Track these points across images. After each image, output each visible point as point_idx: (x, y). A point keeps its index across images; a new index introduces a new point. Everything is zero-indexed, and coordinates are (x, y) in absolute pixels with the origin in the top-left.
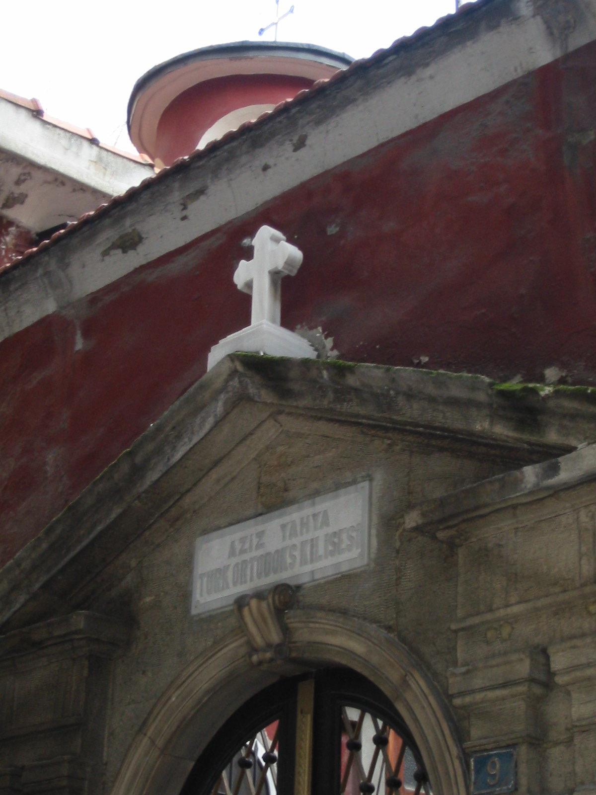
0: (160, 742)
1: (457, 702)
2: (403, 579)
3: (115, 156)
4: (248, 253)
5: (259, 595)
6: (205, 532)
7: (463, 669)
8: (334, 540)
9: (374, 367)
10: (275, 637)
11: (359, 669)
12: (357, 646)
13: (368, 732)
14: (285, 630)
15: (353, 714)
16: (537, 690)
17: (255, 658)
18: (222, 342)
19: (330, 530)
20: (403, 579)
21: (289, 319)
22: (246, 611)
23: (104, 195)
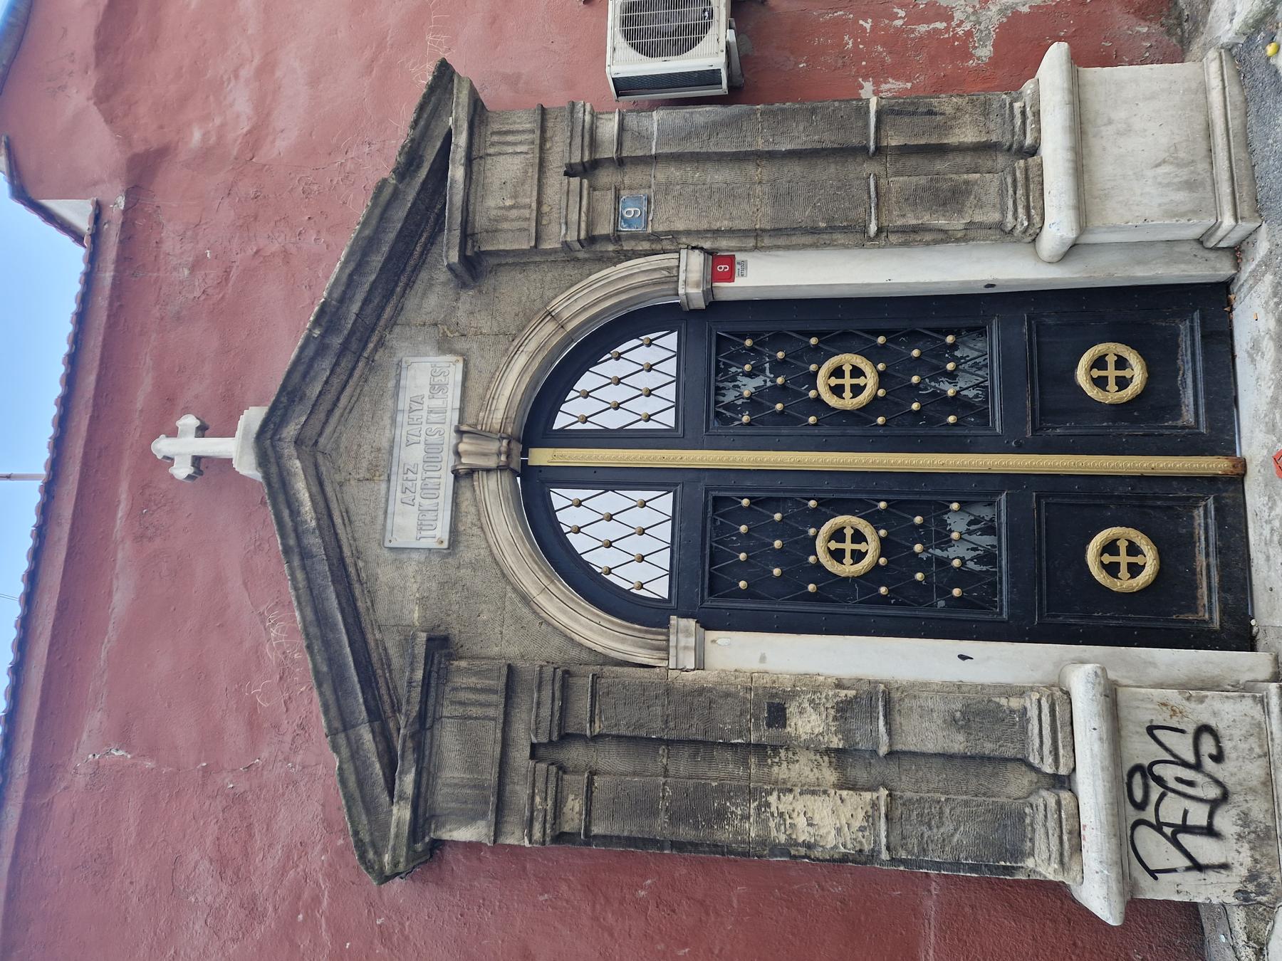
11: (526, 379)
12: (521, 361)
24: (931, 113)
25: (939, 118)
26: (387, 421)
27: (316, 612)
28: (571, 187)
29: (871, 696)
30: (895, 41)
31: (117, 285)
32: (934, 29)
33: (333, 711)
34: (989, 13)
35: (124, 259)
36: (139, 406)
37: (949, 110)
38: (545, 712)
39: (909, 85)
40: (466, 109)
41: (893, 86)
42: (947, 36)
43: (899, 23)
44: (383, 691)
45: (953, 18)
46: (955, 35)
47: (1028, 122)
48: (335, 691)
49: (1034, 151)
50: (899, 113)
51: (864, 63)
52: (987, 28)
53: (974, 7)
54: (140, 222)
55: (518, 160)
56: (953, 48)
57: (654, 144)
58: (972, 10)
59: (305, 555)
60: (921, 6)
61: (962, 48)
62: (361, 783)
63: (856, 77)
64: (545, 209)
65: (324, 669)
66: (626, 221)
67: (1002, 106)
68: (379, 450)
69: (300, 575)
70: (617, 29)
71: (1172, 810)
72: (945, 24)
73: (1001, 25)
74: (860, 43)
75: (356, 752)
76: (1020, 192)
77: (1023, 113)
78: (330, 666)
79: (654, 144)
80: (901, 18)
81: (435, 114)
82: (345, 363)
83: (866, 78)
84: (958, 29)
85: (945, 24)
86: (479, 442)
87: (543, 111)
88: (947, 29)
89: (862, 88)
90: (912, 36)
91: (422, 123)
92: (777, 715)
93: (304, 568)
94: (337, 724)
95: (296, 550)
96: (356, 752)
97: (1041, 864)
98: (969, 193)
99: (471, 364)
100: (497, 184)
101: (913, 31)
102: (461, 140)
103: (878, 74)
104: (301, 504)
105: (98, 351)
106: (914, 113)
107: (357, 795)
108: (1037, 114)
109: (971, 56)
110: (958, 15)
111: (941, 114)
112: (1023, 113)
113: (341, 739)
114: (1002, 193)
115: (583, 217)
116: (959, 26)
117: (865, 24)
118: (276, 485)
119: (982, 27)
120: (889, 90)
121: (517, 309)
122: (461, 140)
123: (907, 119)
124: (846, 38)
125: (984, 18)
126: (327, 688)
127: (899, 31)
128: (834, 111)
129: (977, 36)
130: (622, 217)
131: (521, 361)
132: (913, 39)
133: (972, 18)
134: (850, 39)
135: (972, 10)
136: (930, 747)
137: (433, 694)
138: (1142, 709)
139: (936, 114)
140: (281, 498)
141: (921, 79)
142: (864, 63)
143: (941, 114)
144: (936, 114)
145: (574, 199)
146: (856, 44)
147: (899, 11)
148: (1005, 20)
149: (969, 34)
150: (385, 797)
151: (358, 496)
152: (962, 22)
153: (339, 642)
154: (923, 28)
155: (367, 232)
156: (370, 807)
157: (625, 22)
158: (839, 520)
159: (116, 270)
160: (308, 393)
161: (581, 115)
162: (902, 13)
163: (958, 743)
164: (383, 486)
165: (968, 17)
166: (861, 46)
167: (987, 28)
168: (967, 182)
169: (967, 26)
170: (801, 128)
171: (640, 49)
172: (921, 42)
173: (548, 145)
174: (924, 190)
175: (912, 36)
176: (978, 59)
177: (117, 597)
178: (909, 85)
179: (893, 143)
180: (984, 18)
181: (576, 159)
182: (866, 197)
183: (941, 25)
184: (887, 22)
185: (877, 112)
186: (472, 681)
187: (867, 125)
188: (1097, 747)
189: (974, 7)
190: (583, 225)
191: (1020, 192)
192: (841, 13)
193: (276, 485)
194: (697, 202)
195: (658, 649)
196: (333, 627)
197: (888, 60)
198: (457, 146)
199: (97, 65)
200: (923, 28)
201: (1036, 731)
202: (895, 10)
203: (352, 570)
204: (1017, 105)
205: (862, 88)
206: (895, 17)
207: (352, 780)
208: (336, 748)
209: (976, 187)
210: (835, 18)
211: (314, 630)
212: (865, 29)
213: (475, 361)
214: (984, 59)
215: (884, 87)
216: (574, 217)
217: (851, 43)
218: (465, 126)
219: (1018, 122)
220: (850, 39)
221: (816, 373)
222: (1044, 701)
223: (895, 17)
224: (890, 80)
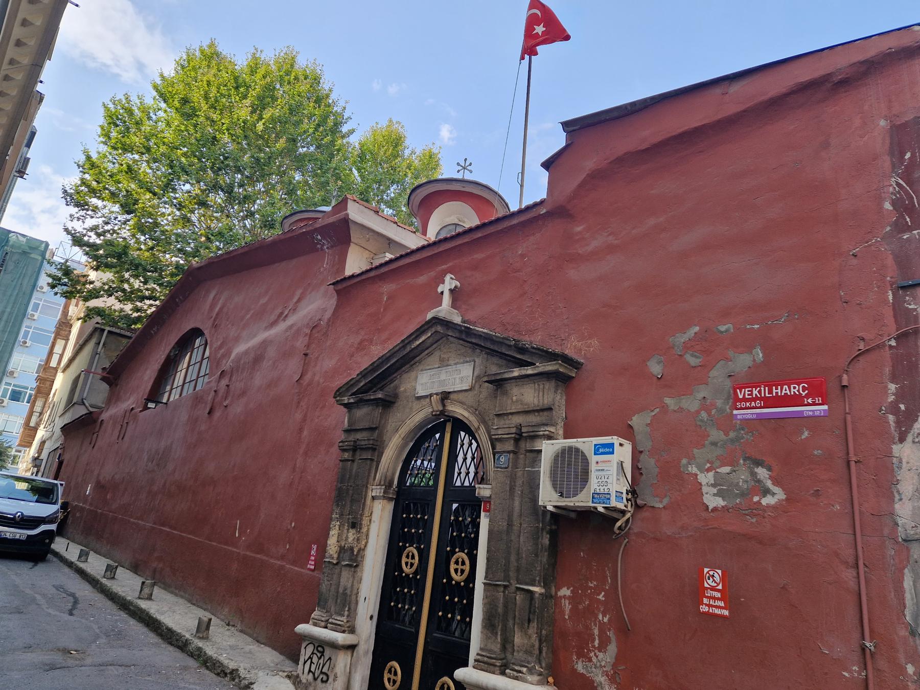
0: (402, 436)
1: (493, 437)
2: (709, 598)
3: (477, 185)
4: (443, 283)
5: (437, 394)
6: (422, 370)
7: (496, 427)
8: (462, 379)
9: (474, 324)
10: (441, 408)
11: (461, 418)
12: (466, 414)
13: (466, 441)
14: (444, 406)
15: (463, 434)
16: (517, 437)
17: (434, 413)
18: (432, 311)
19: (461, 376)
20: (709, 598)
21: (454, 304)
22: (432, 398)
23: (410, 248)
24: (529, 621)
25: (526, 625)
26: (457, 361)
27: (390, 356)
28: (512, 429)
29: (356, 561)
30: (590, 612)
31: (512, 227)
32: (595, 638)
33: (365, 372)
34: (600, 676)
35: (523, 224)
36: (475, 256)
37: (530, 631)
38: (363, 443)
39: (567, 617)
40: (543, 370)
41: (567, 606)
42: (590, 645)
43: (600, 617)
44: (383, 384)
45: (600, 651)
46: (590, 651)
47: (515, 673)
48: (370, 371)
49: (503, 673)
50: (531, 604)
51: (580, 592)
52: (592, 672)
53: (605, 667)
54: (540, 223)
55: (532, 399)
56: (583, 649)
57: (530, 469)
58: (603, 665)
59: (404, 347)
60: (608, 633)
61: (583, 655)
62: (352, 385)
63: (573, 586)
64: (510, 417)
65: (375, 365)
66: (499, 457)
67: (528, 662)
68: (448, 360)
69: (398, 348)
70: (567, 445)
71: (315, 659)
72: (597, 646)
73: (593, 682)
74: (591, 591)
75: (359, 381)
76: (486, 659)
77: (520, 672)
78: (376, 367)
79: (530, 469)
80: (603, 619)
81: (541, 356)
82: (412, 355)
83: (572, 592)
84: (593, 654)
85: (597, 646)
86: (440, 402)
87: (550, 409)
88: (594, 646)
89: (568, 589)
90: (593, 624)
91: (534, 351)
92: (353, 526)
93: (400, 349)
94: (363, 373)
95: (405, 343)
96: (359, 381)
97: (316, 614)
98: (492, 634)
99: (470, 392)
100: (522, 391)
101: (595, 625)
102: (529, 371)
103: (573, 599)
104: (418, 340)
105: (489, 232)
106: (530, 612)
107: (349, 385)
108: (516, 678)
109: (578, 658)
110: (601, 655)
111: (528, 627)
112: (520, 672)
113: (360, 376)
114: (490, 651)
115: (500, 436)
116: (595, 654)
117: (601, 595)
118: (421, 330)
119: (594, 669)
120: (565, 605)
121: (487, 408)
122: (529, 371)
123: (527, 607)
124: (595, 583)
125: (598, 672)
126: (371, 367)
127: (596, 617)
128: (535, 566)
129: (589, 664)
130: (501, 455)
131: (466, 414)
132: (591, 624)
133: (598, 664)
134: (594, 585)
135: (603, 665)
136: (341, 580)
137: (373, 402)
138: (342, 661)
139: (529, 624)
140: (418, 333)
141: (569, 624)
142: (580, 592)
143: (528, 627)
144: (529, 624)
145: (507, 431)
146: (591, 588)
147: (607, 619)
148: (595, 685)
149: (590, 660)
150: (350, 394)
151: (434, 359)
152: (597, 657)
153: (383, 367)
154: (596, 632)
155: (494, 338)
156: (348, 390)
157: (570, 448)
158: (417, 558)
159: (518, 223)
160: (450, 331)
161: (542, 429)
162: (606, 620)
163: (341, 590)
164: (437, 366)
165: (599, 661)
166: (589, 591)
167: (592, 672)
168: (497, 633)
169: (594, 659)
170: (529, 548)
171: (556, 458)
172: (588, 628)
173: (536, 414)
174: (496, 610)
175: (593, 624)
176: (577, 662)
177: (422, 278)
178: (567, 617)
179: (517, 598)
180: (598, 672)
181: (524, 430)
182: (496, 579)
183: (596, 643)
184: (602, 609)
185: (530, 590)
186: (541, 398)
187: (527, 584)
188: (324, 635)
189: (605, 667)
190: (497, 437)
191: (486, 659)
192: (609, 581)
193: (421, 330)
194: (502, 492)
195: (380, 482)
196: (387, 364)
197: (581, 607)
198: (527, 370)
199: (610, 163)
200: (596, 632)
201: (338, 619)
202: (608, 616)
203: (412, 362)
204: (524, 670)
205: (568, 589)
206: (604, 615)
207: (352, 383)
208: (358, 375)
209: (494, 638)
210: (607, 577)
211: (384, 358)
212: (599, 595)
213: (471, 394)
214: (576, 666)
215: (567, 602)
216: (500, 432)
217: (592, 585)
218: (535, 372)
219: (516, 668)
220: (594, 585)
221: (463, 552)
222: (342, 623)
223: (604, 615)
224: (570, 606)
